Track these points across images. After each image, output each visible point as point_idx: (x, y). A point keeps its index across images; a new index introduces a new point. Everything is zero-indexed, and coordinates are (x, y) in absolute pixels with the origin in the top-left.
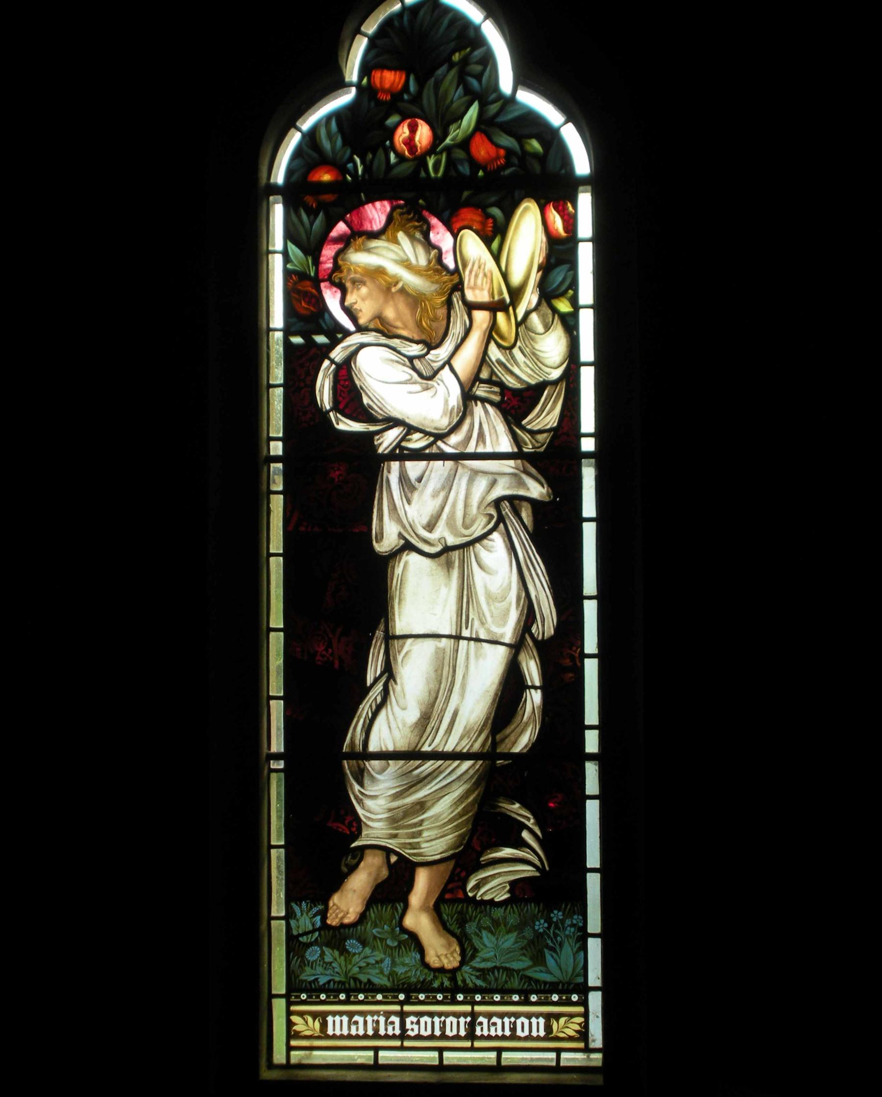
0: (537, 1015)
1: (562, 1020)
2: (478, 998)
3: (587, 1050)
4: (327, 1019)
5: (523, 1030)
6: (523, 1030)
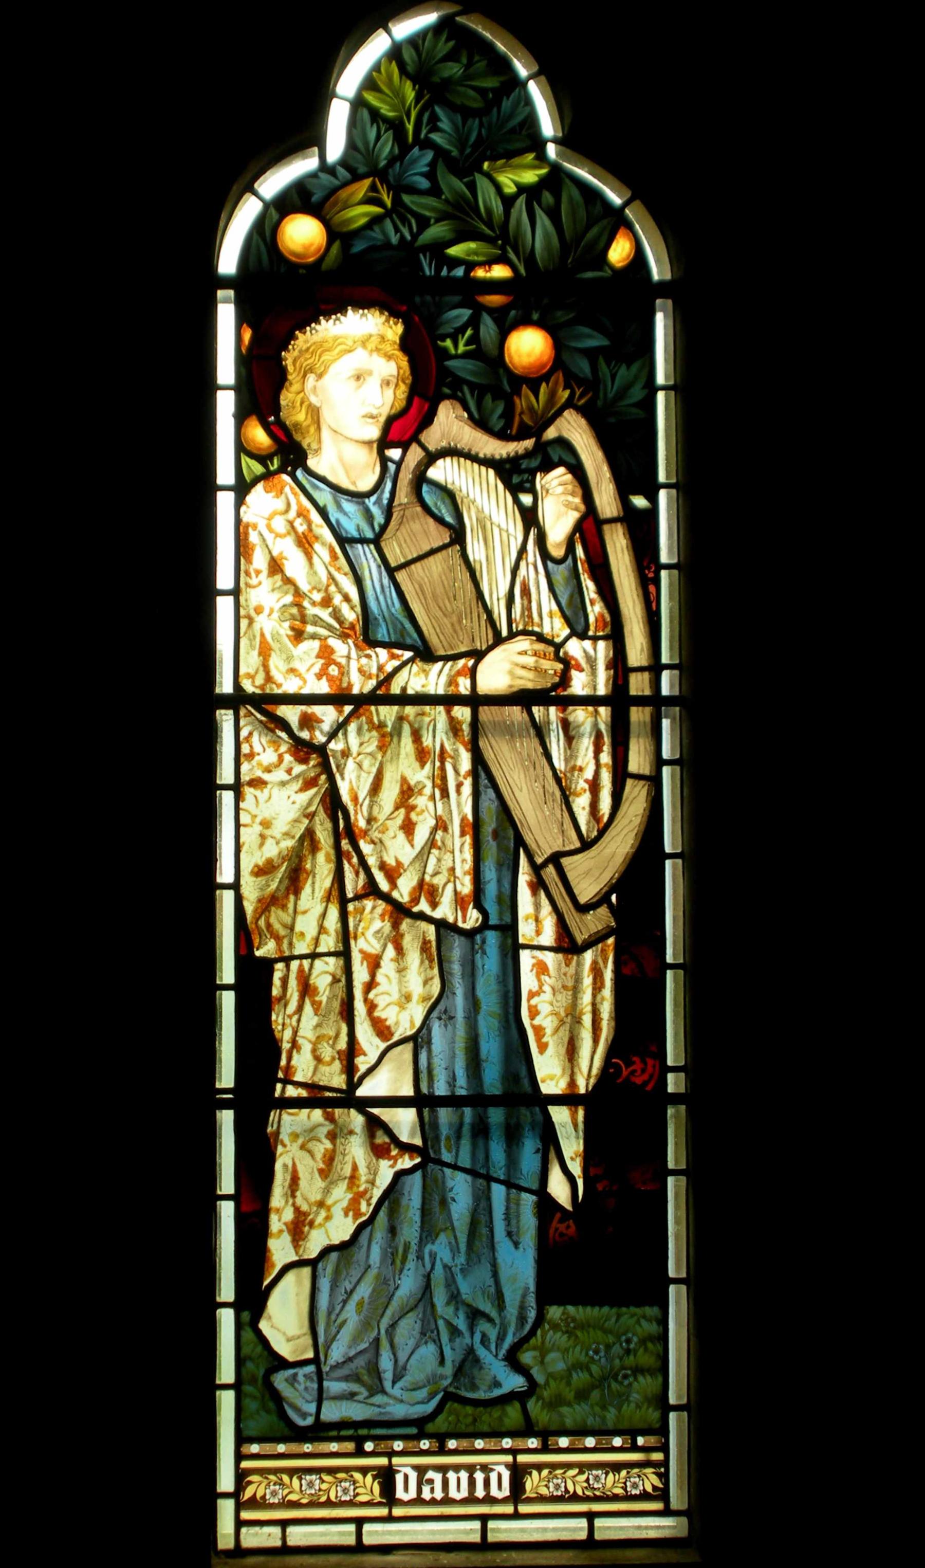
0: (457, 1468)
1: (545, 1472)
2: (398, 1445)
3: (667, 1512)
4: (474, 1476)
5: (406, 1489)
6: (406, 1489)
